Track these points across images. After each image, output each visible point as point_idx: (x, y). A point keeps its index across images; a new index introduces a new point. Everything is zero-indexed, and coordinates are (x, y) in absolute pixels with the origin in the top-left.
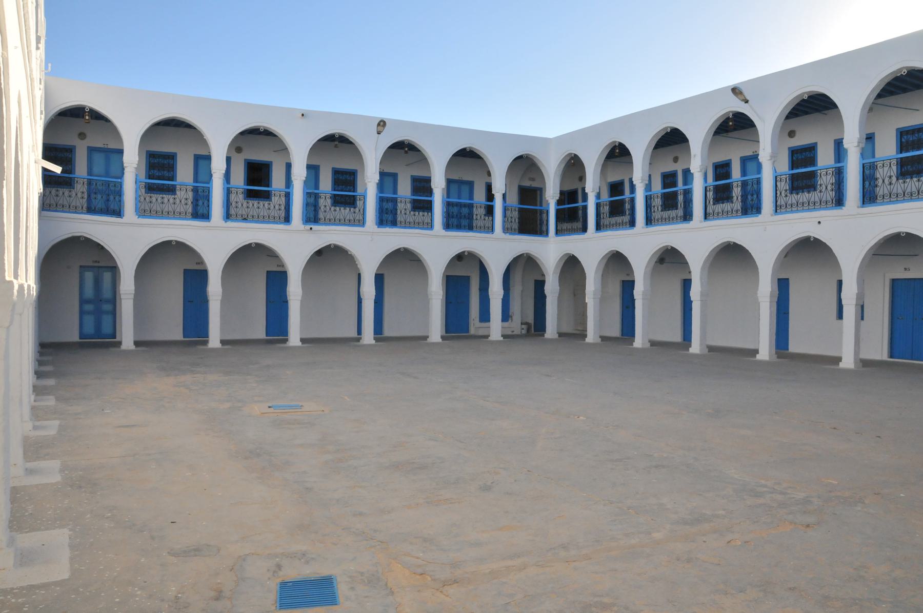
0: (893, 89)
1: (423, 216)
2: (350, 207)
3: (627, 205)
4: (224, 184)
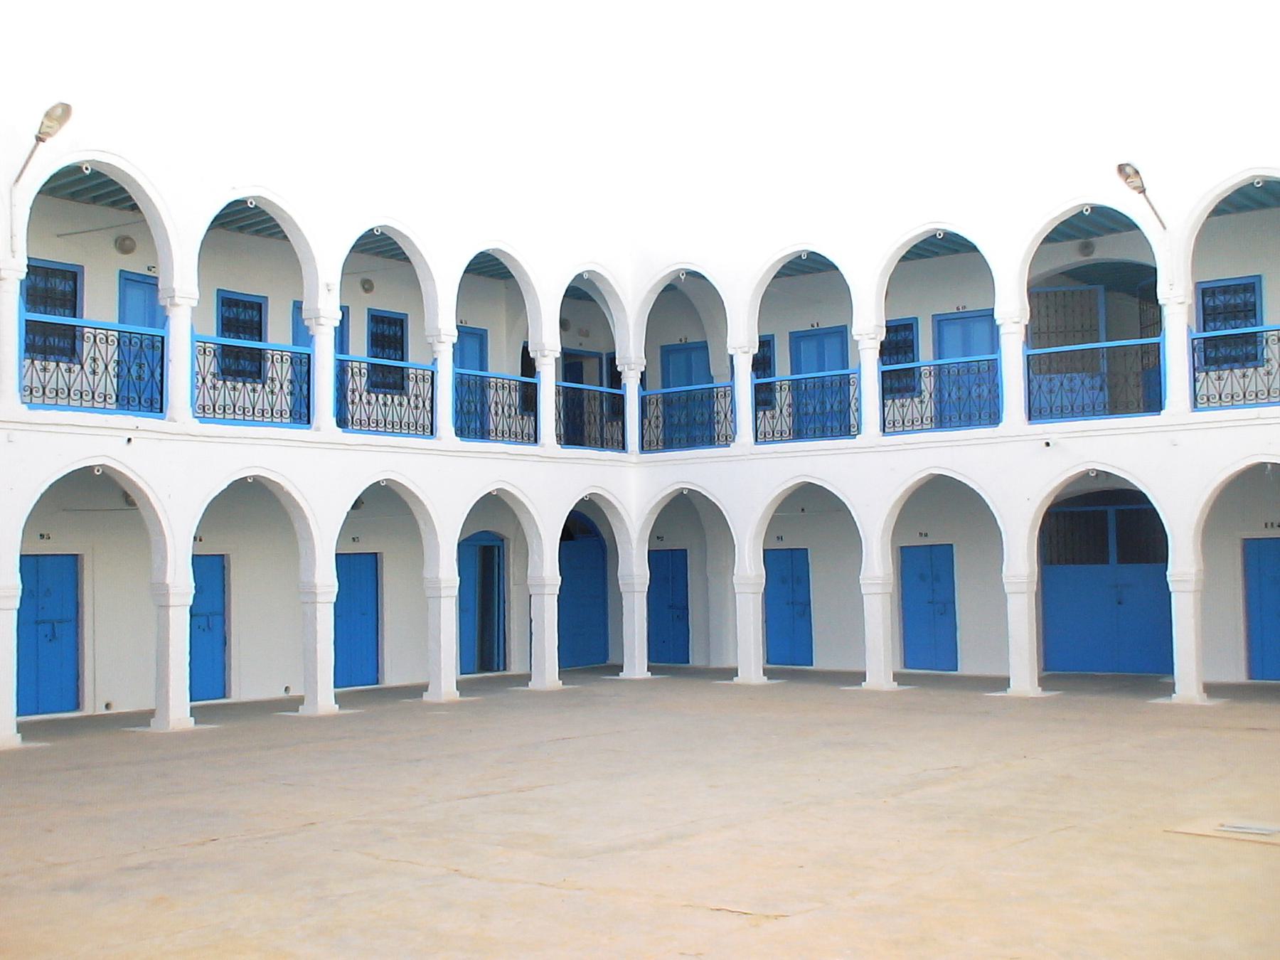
0: (789, 272)
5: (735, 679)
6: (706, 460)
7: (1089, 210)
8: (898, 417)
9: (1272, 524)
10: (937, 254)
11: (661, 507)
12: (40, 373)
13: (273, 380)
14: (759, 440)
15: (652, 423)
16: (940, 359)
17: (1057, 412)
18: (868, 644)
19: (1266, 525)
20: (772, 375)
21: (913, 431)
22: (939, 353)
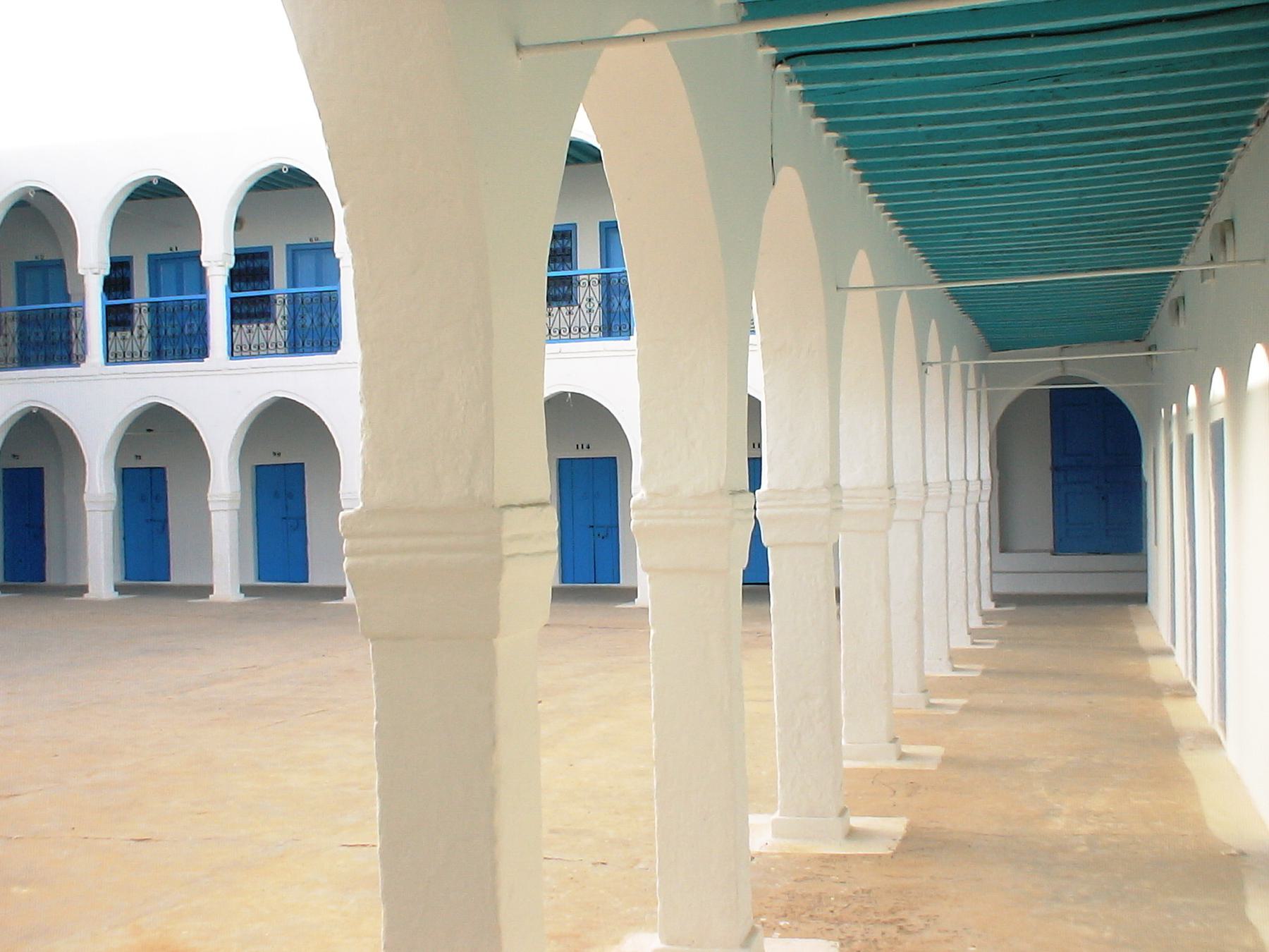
3: (278, 308)
5: (86, 595)
6: (52, 379)
7: (287, 170)
8: (119, 350)
10: (291, 187)
11: (10, 425)
12: (566, 316)
14: (110, 361)
15: (315, 321)
16: (607, 267)
17: (308, 346)
18: (216, 559)
21: (259, 356)
22: (293, 282)
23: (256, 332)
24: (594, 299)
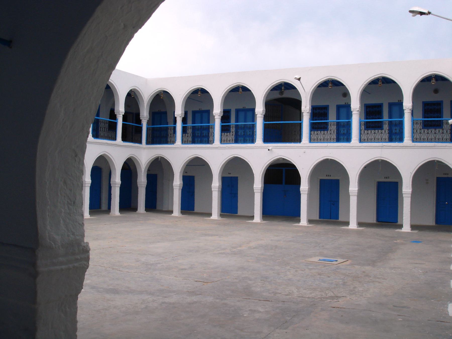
1: (227, 136)
2: (378, 130)
4: (182, 125)
9: (328, 175)
13: (188, 133)
19: (327, 175)
20: (229, 122)
23: (321, 134)
24: (332, 130)
